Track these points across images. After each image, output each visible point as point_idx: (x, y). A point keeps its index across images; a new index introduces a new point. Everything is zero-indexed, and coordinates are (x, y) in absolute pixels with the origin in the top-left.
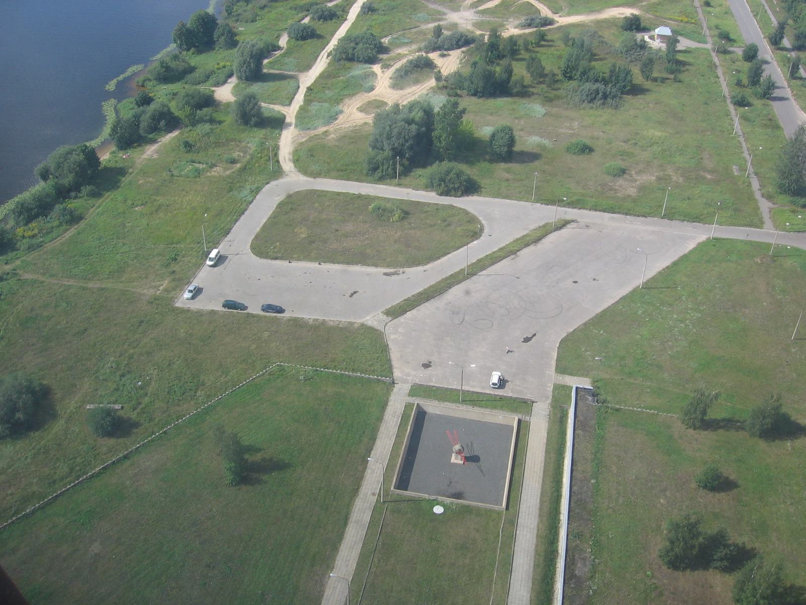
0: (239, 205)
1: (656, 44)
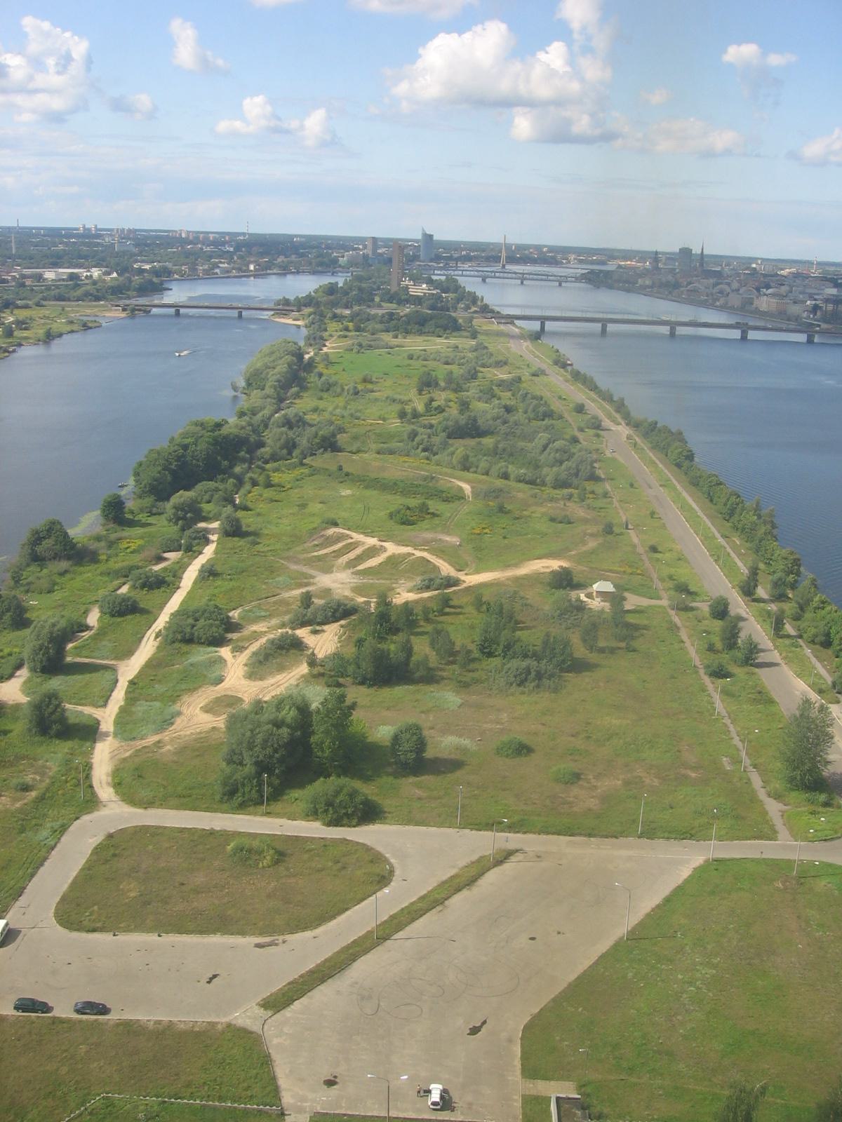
0: (35, 851)
1: (596, 604)
